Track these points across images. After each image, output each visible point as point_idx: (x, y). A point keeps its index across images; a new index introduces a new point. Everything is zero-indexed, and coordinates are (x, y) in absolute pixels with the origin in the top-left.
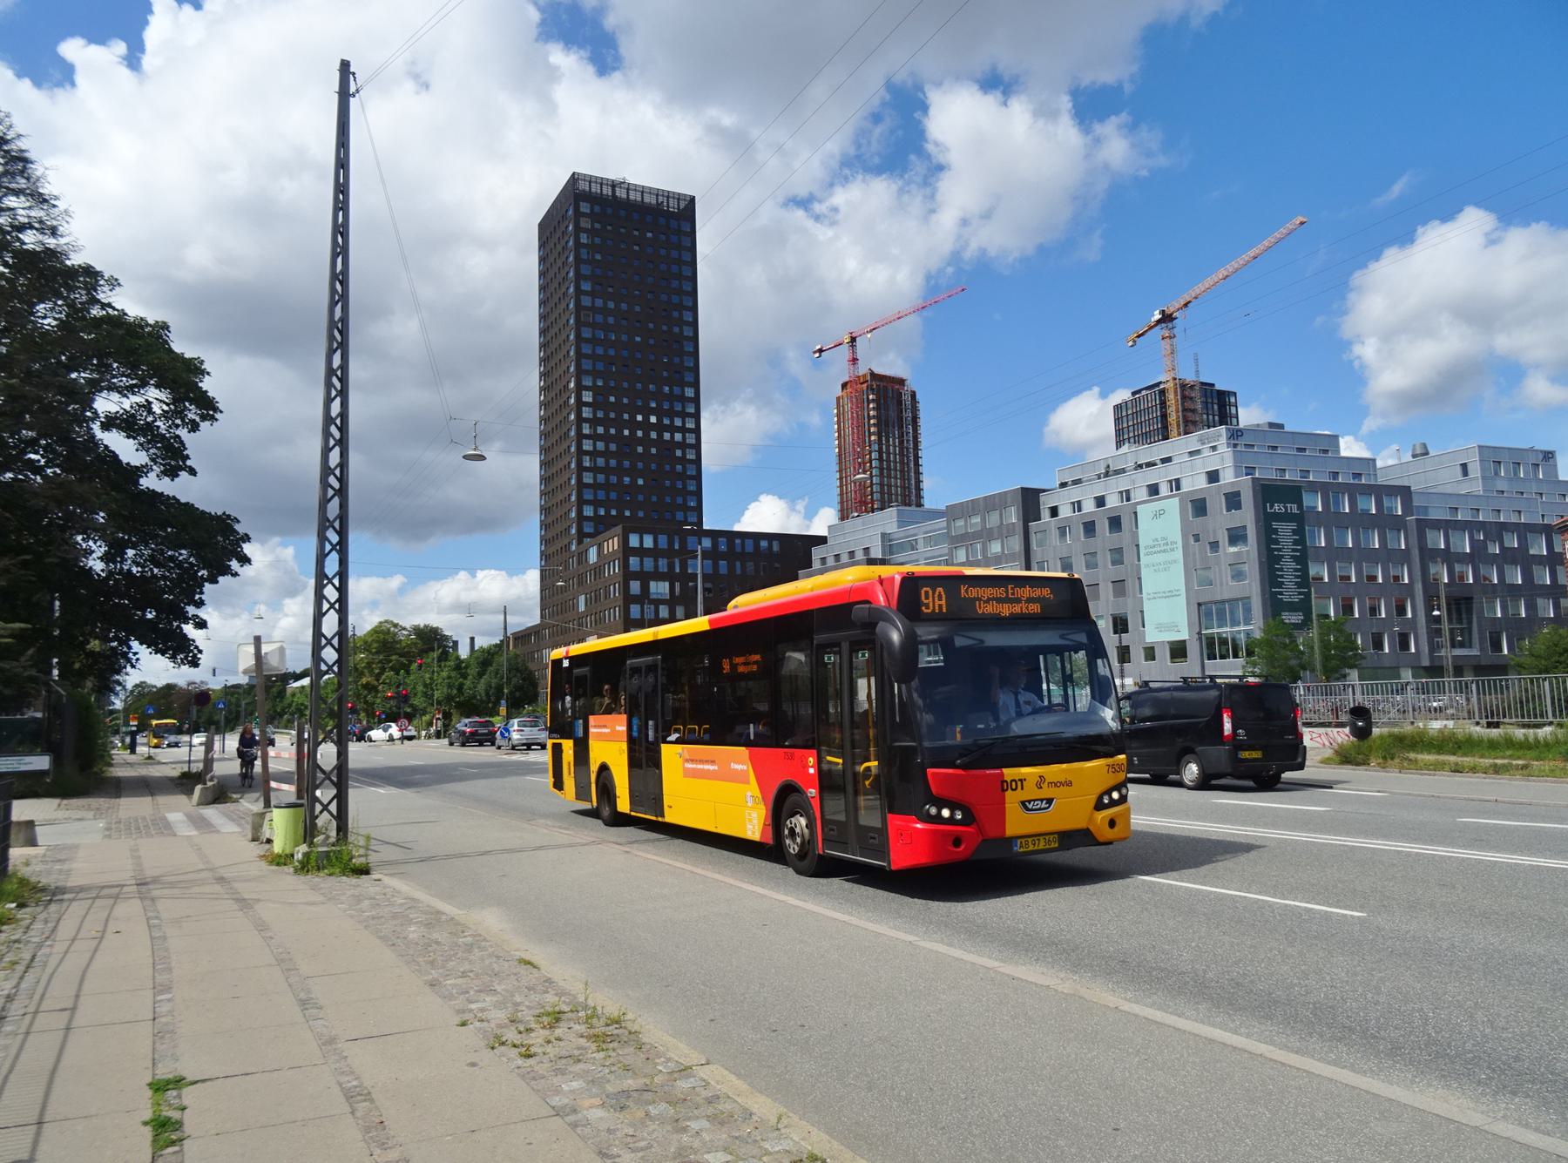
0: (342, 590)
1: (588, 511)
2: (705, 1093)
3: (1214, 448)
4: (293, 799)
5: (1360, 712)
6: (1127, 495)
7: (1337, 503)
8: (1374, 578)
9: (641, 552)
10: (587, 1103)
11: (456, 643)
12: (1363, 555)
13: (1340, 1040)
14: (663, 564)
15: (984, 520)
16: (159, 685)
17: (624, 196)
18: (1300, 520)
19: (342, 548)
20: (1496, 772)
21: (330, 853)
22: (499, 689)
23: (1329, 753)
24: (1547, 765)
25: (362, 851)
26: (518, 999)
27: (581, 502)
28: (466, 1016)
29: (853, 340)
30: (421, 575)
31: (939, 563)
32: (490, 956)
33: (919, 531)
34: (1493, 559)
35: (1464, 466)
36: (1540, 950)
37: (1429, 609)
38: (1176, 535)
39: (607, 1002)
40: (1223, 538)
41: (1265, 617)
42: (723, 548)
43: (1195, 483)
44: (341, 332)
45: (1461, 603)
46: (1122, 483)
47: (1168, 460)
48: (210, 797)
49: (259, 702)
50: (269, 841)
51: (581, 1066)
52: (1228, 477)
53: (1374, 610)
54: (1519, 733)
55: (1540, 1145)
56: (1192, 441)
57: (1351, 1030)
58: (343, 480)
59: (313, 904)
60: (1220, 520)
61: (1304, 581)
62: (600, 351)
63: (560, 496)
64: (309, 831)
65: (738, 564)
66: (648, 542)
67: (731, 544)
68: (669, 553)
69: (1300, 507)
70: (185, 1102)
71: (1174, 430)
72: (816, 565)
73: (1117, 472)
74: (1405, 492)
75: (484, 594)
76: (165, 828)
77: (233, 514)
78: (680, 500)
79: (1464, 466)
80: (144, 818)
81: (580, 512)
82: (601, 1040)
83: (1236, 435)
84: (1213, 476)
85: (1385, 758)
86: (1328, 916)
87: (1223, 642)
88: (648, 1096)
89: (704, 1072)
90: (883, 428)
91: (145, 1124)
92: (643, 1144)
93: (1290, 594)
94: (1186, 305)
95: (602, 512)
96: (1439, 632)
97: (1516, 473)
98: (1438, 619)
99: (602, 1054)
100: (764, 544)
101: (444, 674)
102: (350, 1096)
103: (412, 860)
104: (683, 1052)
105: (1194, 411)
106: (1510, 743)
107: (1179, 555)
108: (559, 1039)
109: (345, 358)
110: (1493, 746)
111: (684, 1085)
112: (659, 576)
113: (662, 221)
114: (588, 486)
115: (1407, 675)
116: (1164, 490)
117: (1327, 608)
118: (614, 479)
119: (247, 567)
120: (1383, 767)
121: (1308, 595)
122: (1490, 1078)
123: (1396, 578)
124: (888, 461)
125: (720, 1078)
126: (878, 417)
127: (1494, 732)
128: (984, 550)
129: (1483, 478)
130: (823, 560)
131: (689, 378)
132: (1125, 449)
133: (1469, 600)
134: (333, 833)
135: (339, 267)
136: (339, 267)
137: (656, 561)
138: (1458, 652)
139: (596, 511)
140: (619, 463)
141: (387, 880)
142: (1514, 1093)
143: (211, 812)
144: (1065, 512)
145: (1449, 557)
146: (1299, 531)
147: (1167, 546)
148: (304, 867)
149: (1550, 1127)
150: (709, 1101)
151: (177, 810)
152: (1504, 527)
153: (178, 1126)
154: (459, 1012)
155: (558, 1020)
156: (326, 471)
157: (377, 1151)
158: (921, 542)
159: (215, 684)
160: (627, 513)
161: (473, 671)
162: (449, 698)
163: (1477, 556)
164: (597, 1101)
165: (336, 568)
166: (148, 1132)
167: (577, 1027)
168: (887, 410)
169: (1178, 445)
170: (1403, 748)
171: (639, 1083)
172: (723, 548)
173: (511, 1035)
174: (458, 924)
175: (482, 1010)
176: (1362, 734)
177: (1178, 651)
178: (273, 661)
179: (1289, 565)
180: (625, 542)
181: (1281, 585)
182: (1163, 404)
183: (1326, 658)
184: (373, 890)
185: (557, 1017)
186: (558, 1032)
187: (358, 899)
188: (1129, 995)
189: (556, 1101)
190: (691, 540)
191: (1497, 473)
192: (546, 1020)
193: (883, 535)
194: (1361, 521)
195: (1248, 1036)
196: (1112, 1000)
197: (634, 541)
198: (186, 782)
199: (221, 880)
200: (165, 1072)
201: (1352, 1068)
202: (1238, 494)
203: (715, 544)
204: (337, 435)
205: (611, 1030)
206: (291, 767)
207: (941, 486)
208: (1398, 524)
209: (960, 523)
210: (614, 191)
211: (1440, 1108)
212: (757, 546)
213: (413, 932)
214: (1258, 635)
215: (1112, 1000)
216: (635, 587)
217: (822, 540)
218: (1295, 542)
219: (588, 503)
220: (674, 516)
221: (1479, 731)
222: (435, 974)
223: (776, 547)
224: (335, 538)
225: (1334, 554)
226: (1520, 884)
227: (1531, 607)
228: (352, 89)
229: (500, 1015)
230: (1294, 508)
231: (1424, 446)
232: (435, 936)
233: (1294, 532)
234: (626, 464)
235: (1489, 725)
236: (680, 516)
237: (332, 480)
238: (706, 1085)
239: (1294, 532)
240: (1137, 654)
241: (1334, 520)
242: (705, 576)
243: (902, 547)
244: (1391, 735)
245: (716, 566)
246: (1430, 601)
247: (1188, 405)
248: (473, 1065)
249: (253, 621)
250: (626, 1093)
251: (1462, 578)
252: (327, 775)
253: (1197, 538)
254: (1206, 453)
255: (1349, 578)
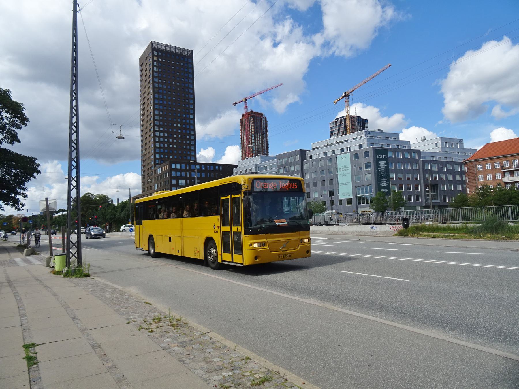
0: (78, 182)
1: (158, 156)
2: (212, 341)
3: (361, 137)
4: (61, 252)
5: (405, 220)
6: (334, 152)
7: (398, 155)
8: (409, 178)
9: (176, 170)
10: (173, 345)
11: (112, 200)
12: (406, 171)
13: (403, 317)
14: (183, 174)
15: (288, 160)
16: (7, 215)
17: (169, 50)
18: (387, 160)
19: (77, 168)
20: (445, 238)
21: (76, 270)
22: (128, 215)
23: (396, 232)
24: (460, 235)
25: (87, 270)
26: (146, 314)
27: (155, 153)
28: (129, 321)
29: (246, 100)
30: (104, 176)
31: (274, 174)
32: (135, 301)
33: (268, 163)
34: (444, 173)
35: (436, 144)
36: (460, 289)
37: (425, 188)
38: (349, 165)
39: (176, 315)
40: (364, 166)
41: (376, 191)
42: (203, 169)
43: (355, 148)
44: (75, 94)
45: (435, 186)
46: (332, 148)
47: (347, 141)
48: (30, 253)
49: (47, 220)
50: (53, 267)
51: (169, 334)
52: (365, 147)
53: (409, 189)
54: (452, 226)
55: (462, 344)
56: (354, 135)
57: (406, 314)
58: (77, 144)
59: (72, 287)
60: (363, 160)
61: (388, 179)
62: (161, 102)
63: (148, 151)
64: (68, 264)
65: (208, 174)
66: (178, 166)
67: (206, 167)
68: (185, 170)
69: (387, 156)
70: (37, 351)
71: (348, 131)
72: (234, 173)
73: (330, 145)
74: (418, 151)
75: (123, 183)
76: (15, 264)
77: (35, 157)
78: (189, 153)
79: (436, 144)
80: (6, 261)
81: (155, 156)
82: (175, 326)
83: (368, 133)
84: (361, 146)
85: (413, 234)
86: (398, 281)
87: (363, 199)
88: (192, 342)
89: (210, 334)
90: (255, 129)
91: (24, 358)
92: (192, 357)
93: (384, 183)
94: (353, 91)
95: (162, 156)
96: (428, 195)
97: (451, 146)
98: (428, 191)
99: (176, 330)
100: (217, 167)
101: (110, 211)
102: (93, 347)
103: (103, 272)
104: (202, 329)
105: (355, 125)
106: (449, 229)
107: (350, 171)
108: (161, 326)
109: (77, 103)
110: (444, 230)
111: (204, 338)
112: (182, 178)
113: (182, 59)
114: (157, 148)
115: (418, 209)
116: (345, 151)
117: (395, 188)
118: (166, 145)
119: (39, 175)
120: (412, 236)
121: (389, 184)
122: (447, 326)
123: (416, 179)
124: (258, 140)
125: (215, 336)
126: (254, 126)
127: (445, 225)
128: (289, 170)
129: (442, 147)
130: (236, 173)
131: (192, 112)
132: (333, 137)
133: (437, 185)
134: (76, 264)
135: (74, 72)
136: (74, 72)
137: (181, 173)
138: (434, 201)
139: (160, 156)
140: (168, 140)
141: (96, 279)
142: (454, 330)
143: (30, 258)
144: (314, 157)
145: (431, 172)
146: (387, 164)
147: (346, 168)
148: (67, 275)
149: (464, 339)
150: (212, 343)
151: (18, 258)
152: (448, 163)
153: (36, 358)
154: (127, 319)
155: (160, 320)
156: (71, 141)
157: (105, 363)
158: (268, 167)
159: (28, 215)
160: (171, 157)
161: (119, 210)
162: (111, 219)
163: (440, 172)
164: (176, 345)
165: (75, 175)
166: (25, 361)
167: (167, 322)
168: (257, 123)
169: (350, 136)
170: (418, 231)
171: (189, 338)
172: (203, 169)
173: (145, 326)
174: (122, 292)
175: (135, 318)
176: (406, 226)
177: (349, 201)
178: (52, 207)
179: (383, 174)
180: (170, 166)
181: (381, 181)
182: (345, 123)
183: (395, 203)
184: (92, 282)
185: (160, 319)
186: (160, 324)
187: (87, 285)
188: (340, 306)
189: (162, 345)
190: (193, 167)
191: (446, 146)
192: (156, 320)
193: (256, 164)
194: (405, 161)
195: (376, 317)
196: (335, 308)
197: (173, 166)
198: (20, 248)
199: (37, 280)
200: (28, 342)
201: (407, 325)
202: (368, 152)
203: (201, 168)
204: (75, 129)
205: (178, 323)
206: (60, 242)
207: (275, 149)
208: (416, 162)
209: (281, 161)
210: (165, 48)
211: (433, 335)
212: (214, 168)
213: (108, 295)
214: (374, 196)
215: (335, 308)
216: (174, 182)
217: (236, 166)
218: (386, 167)
219: (158, 153)
220: (187, 158)
221: (440, 225)
222: (117, 308)
223: (221, 168)
224: (75, 164)
225: (397, 171)
226: (453, 270)
227: (455, 187)
228: (78, 10)
229: (140, 320)
230: (385, 156)
231: (425, 137)
232: (115, 296)
233: (385, 164)
234: (171, 140)
235: (443, 223)
236: (189, 158)
237: (73, 145)
238: (211, 338)
239: (385, 164)
240: (337, 203)
241: (397, 161)
242: (198, 178)
243: (262, 168)
244: (414, 227)
245: (201, 175)
246: (426, 186)
247: (353, 123)
248: (134, 335)
249: (46, 191)
250: (185, 342)
251: (435, 178)
252: (74, 244)
253: (355, 165)
254: (359, 139)
255: (401, 178)
